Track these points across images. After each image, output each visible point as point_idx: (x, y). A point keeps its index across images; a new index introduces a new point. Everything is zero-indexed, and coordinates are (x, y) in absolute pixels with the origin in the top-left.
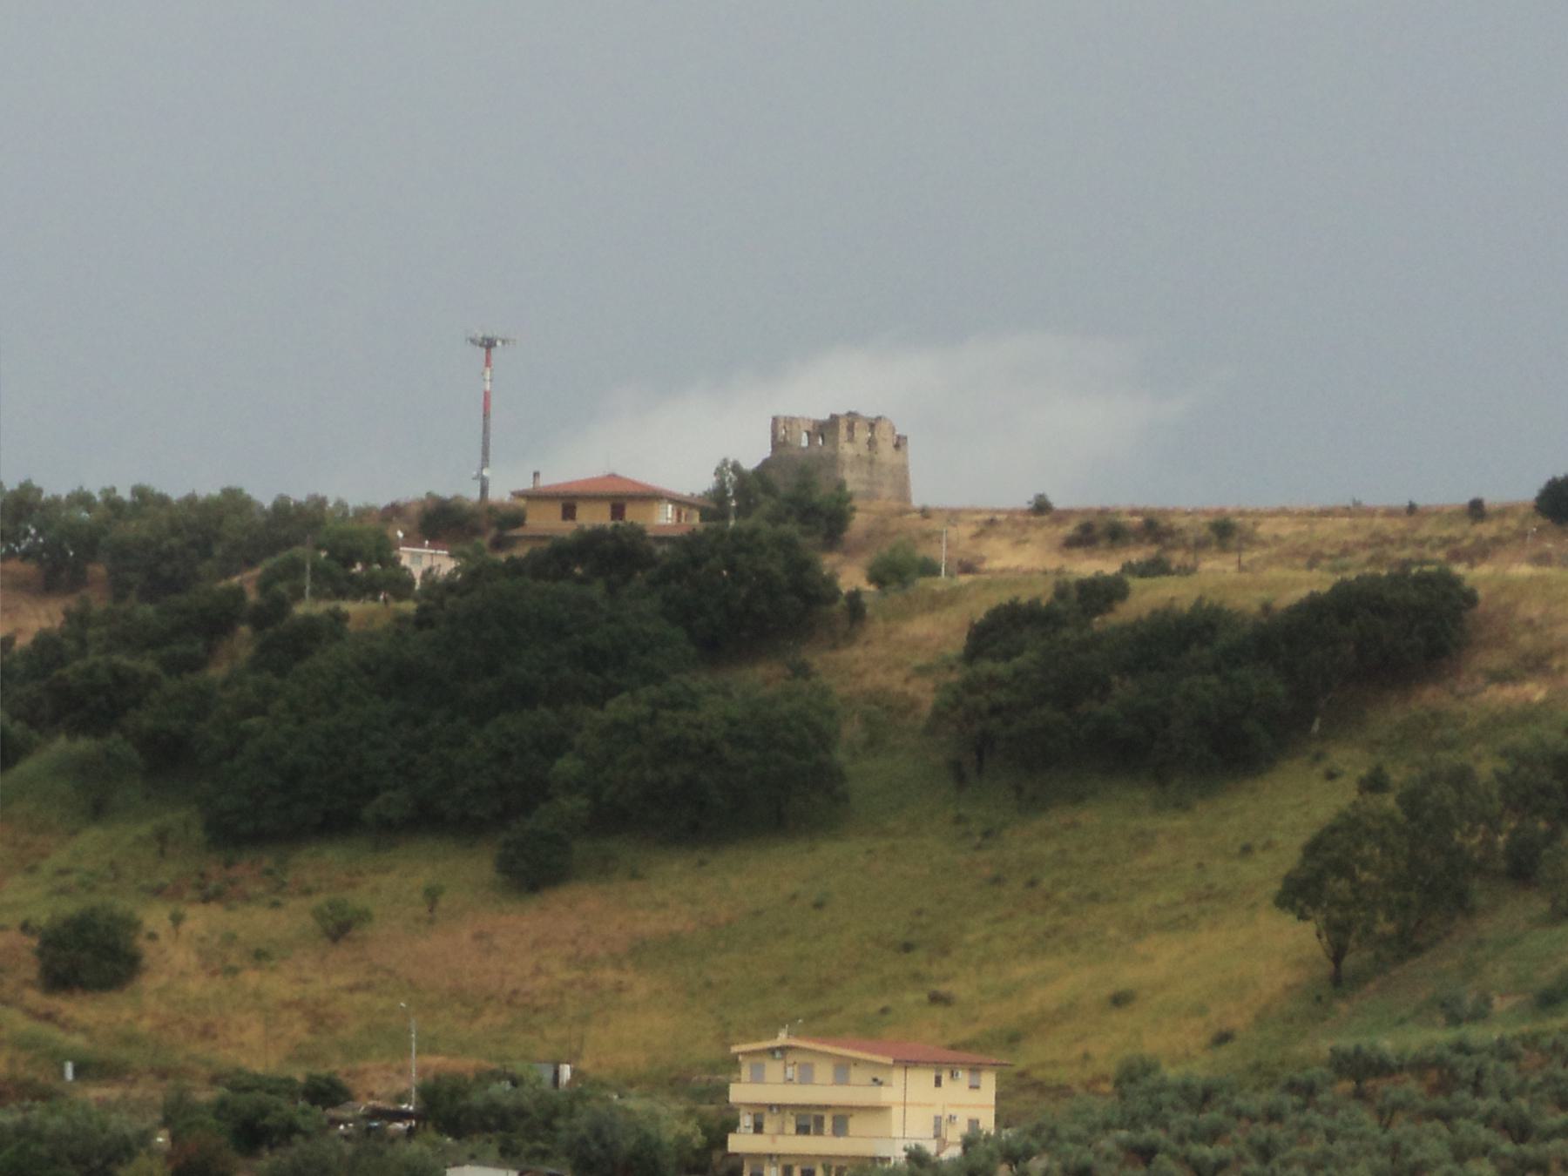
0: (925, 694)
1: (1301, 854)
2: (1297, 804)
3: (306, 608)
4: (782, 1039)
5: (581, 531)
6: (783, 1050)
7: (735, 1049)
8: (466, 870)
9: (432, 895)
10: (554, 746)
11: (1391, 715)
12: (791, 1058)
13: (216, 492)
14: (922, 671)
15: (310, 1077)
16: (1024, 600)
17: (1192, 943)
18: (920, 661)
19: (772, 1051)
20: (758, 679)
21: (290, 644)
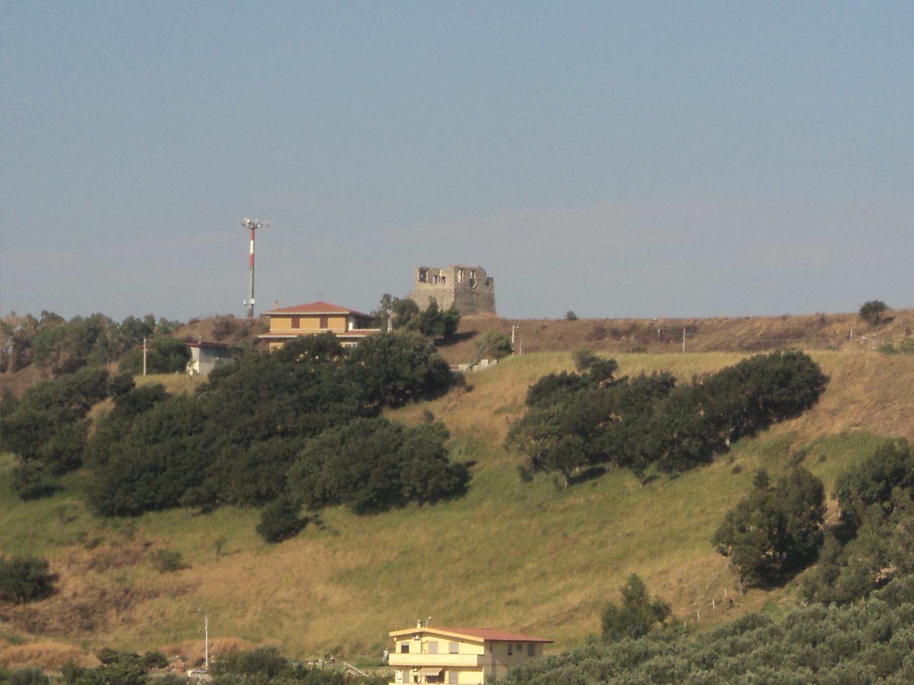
0: (502, 426)
1: (820, 397)
2: (721, 486)
3: (143, 380)
4: (419, 628)
5: (301, 336)
6: (421, 634)
7: (392, 634)
8: (240, 524)
9: (219, 545)
10: (288, 457)
11: (780, 430)
12: (424, 639)
13: (90, 316)
14: (499, 412)
15: (148, 653)
16: (559, 373)
17: (675, 543)
18: (500, 404)
19: (414, 635)
20: (409, 416)
21: (135, 402)
